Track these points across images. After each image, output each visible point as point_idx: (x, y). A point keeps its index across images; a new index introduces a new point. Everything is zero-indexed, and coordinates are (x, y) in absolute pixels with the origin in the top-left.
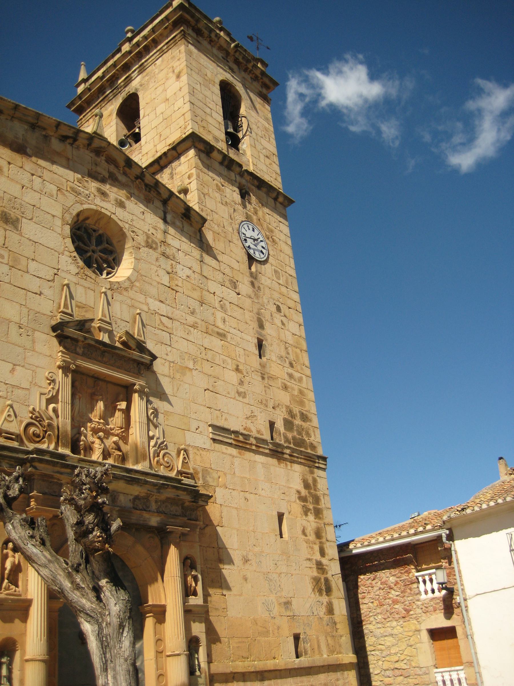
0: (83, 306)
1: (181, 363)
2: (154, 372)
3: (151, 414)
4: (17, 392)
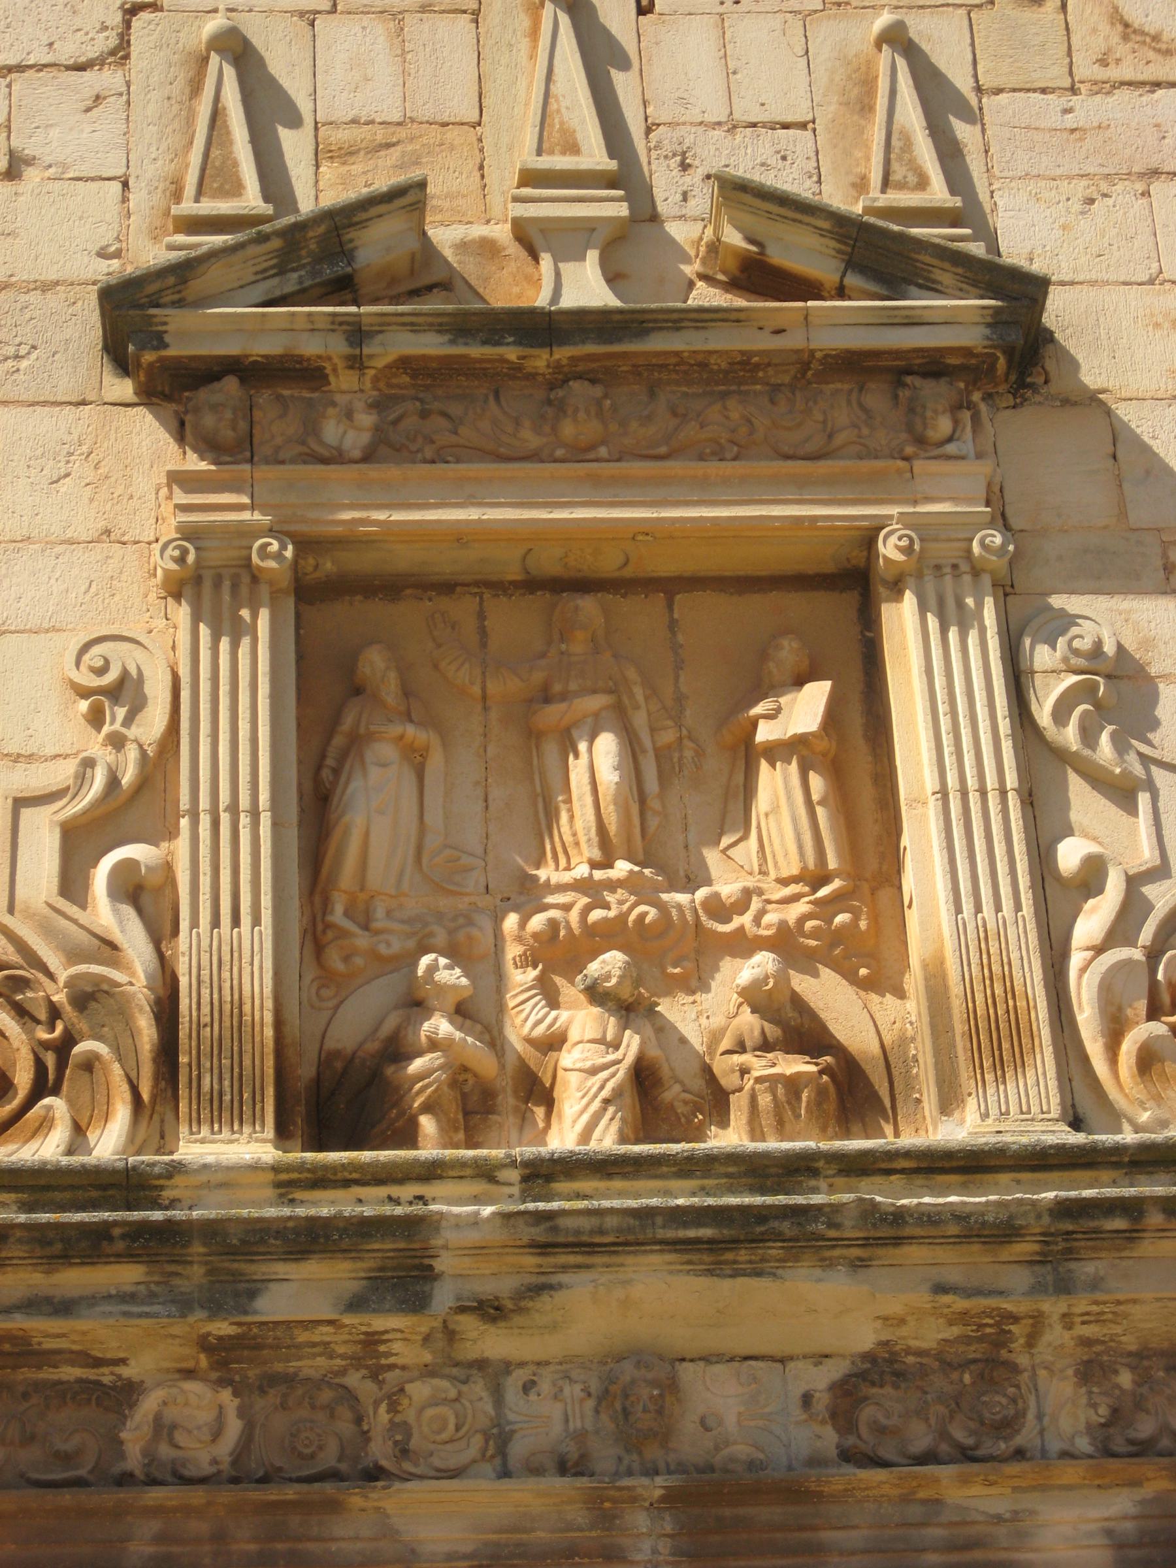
0: (380, 135)
2: (1092, 403)
3: (1061, 713)
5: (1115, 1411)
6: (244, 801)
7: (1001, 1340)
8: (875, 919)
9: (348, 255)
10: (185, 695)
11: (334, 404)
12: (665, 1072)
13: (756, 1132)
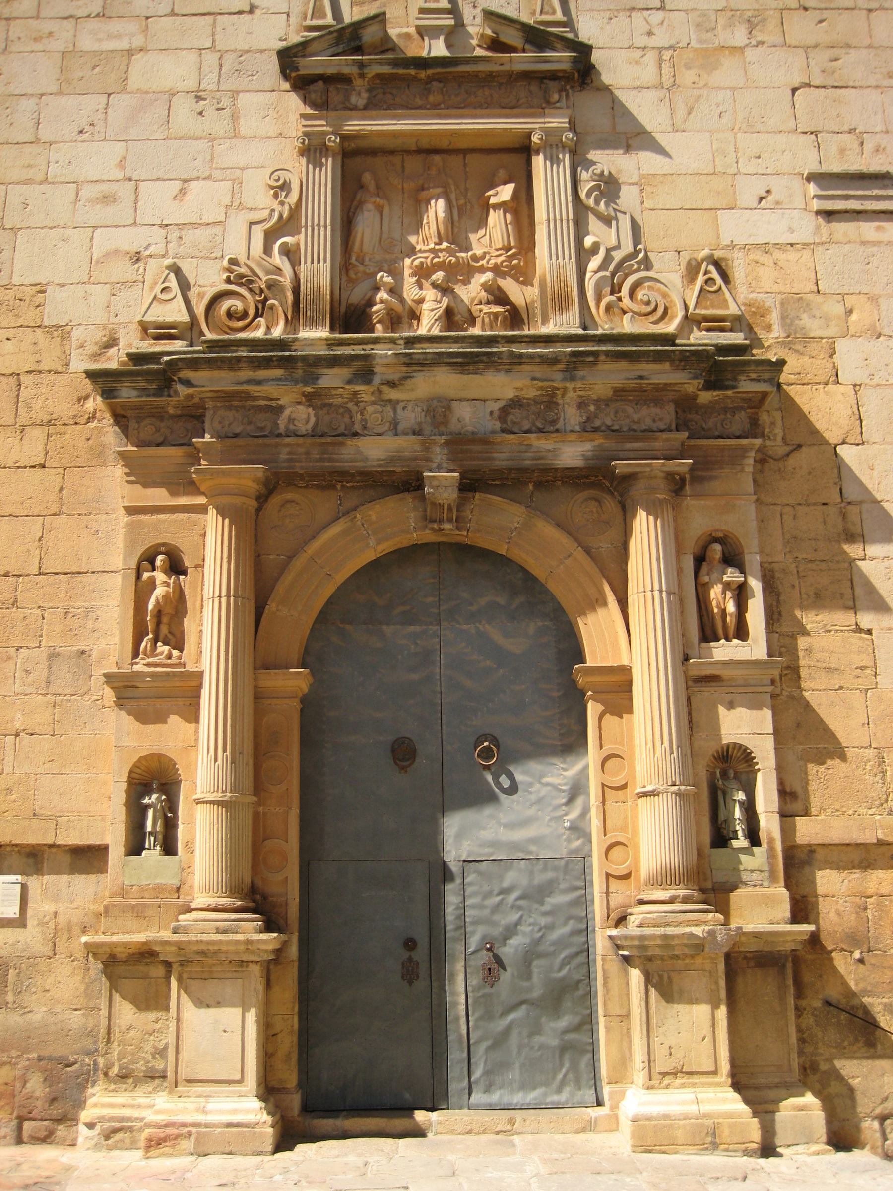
1: (700, 41)
3: (588, 195)
4: (190, 235)
5: (588, 418)
6: (322, 223)
7: (553, 395)
8: (526, 262)
9: (359, 38)
10: (304, 188)
11: (354, 90)
12: (456, 311)
13: (483, 330)
